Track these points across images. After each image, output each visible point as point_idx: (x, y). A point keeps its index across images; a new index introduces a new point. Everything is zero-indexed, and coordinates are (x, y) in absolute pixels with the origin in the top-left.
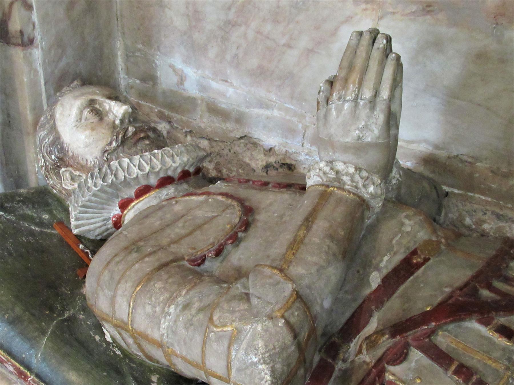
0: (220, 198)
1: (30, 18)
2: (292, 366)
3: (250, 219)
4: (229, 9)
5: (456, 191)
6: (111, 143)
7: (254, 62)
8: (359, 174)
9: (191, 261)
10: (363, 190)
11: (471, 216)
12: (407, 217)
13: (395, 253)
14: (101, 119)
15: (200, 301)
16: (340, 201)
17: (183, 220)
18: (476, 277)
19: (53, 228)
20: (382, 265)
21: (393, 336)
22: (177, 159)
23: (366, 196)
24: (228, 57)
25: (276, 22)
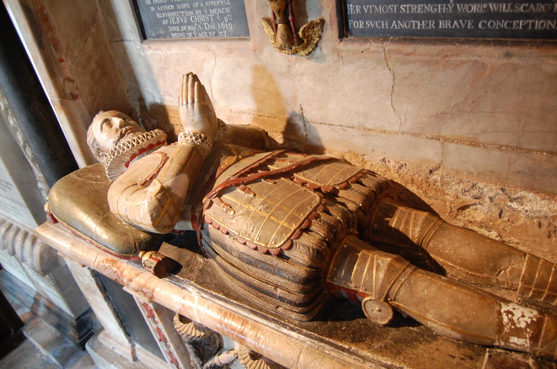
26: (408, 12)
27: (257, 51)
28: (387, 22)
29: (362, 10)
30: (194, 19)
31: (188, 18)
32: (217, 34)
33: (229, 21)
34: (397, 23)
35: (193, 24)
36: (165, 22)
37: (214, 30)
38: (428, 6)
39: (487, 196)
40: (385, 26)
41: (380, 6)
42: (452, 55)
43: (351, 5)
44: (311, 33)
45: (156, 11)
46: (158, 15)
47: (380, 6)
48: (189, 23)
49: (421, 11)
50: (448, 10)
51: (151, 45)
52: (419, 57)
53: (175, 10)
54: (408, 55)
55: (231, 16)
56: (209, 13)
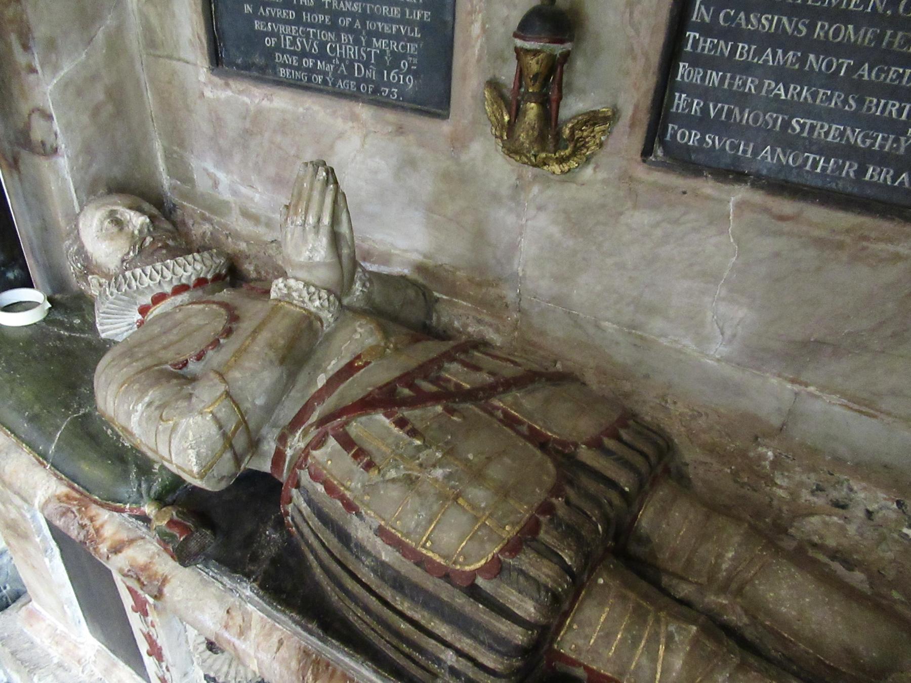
0: (214, 306)
1: (51, 128)
2: (217, 451)
3: (234, 326)
4: (245, 118)
5: (445, 297)
6: (129, 253)
7: (271, 170)
8: (308, 289)
9: (174, 365)
10: (310, 304)
11: (458, 320)
12: (360, 326)
13: (342, 357)
14: (121, 229)
15: (160, 400)
16: (287, 314)
17: (179, 327)
18: (400, 379)
19: (83, 332)
20: (329, 368)
21: (317, 428)
22: (189, 268)
23: (313, 310)
24: (250, 164)
25: (284, 133)
26: (805, 134)
27: (458, 142)
28: (751, 145)
29: (705, 110)
30: (333, 50)
31: (322, 45)
32: (376, 91)
33: (409, 71)
34: (773, 151)
35: (329, 60)
36: (270, 42)
37: (373, 82)
38: (854, 132)
39: (862, 507)
40: (745, 152)
41: (747, 111)
42: (878, 240)
43: (684, 96)
44: (585, 134)
45: (255, 15)
46: (258, 25)
47: (747, 111)
48: (322, 55)
49: (834, 138)
50: (898, 148)
51: (231, 82)
52: (805, 228)
53: (298, 21)
54: (782, 218)
55: (415, 61)
56: (369, 44)
